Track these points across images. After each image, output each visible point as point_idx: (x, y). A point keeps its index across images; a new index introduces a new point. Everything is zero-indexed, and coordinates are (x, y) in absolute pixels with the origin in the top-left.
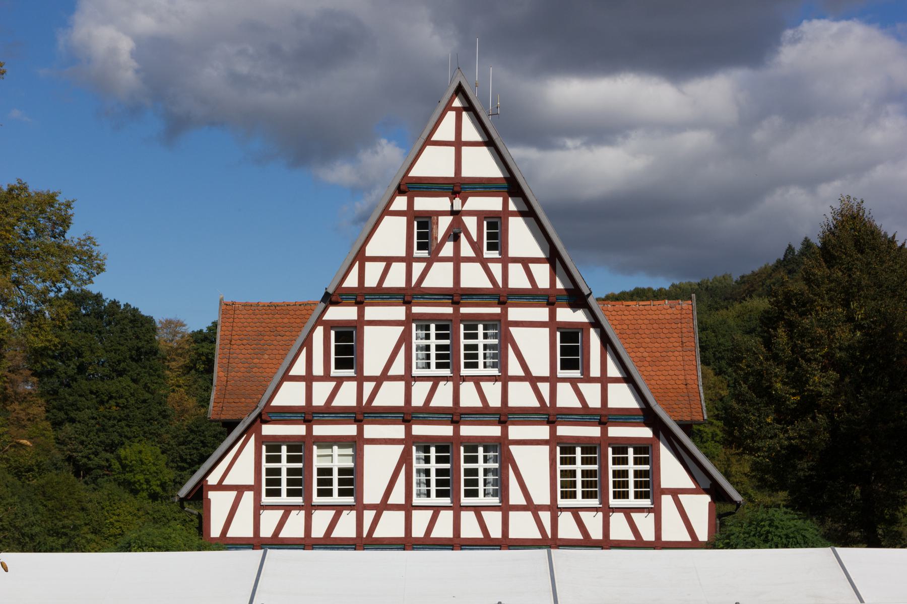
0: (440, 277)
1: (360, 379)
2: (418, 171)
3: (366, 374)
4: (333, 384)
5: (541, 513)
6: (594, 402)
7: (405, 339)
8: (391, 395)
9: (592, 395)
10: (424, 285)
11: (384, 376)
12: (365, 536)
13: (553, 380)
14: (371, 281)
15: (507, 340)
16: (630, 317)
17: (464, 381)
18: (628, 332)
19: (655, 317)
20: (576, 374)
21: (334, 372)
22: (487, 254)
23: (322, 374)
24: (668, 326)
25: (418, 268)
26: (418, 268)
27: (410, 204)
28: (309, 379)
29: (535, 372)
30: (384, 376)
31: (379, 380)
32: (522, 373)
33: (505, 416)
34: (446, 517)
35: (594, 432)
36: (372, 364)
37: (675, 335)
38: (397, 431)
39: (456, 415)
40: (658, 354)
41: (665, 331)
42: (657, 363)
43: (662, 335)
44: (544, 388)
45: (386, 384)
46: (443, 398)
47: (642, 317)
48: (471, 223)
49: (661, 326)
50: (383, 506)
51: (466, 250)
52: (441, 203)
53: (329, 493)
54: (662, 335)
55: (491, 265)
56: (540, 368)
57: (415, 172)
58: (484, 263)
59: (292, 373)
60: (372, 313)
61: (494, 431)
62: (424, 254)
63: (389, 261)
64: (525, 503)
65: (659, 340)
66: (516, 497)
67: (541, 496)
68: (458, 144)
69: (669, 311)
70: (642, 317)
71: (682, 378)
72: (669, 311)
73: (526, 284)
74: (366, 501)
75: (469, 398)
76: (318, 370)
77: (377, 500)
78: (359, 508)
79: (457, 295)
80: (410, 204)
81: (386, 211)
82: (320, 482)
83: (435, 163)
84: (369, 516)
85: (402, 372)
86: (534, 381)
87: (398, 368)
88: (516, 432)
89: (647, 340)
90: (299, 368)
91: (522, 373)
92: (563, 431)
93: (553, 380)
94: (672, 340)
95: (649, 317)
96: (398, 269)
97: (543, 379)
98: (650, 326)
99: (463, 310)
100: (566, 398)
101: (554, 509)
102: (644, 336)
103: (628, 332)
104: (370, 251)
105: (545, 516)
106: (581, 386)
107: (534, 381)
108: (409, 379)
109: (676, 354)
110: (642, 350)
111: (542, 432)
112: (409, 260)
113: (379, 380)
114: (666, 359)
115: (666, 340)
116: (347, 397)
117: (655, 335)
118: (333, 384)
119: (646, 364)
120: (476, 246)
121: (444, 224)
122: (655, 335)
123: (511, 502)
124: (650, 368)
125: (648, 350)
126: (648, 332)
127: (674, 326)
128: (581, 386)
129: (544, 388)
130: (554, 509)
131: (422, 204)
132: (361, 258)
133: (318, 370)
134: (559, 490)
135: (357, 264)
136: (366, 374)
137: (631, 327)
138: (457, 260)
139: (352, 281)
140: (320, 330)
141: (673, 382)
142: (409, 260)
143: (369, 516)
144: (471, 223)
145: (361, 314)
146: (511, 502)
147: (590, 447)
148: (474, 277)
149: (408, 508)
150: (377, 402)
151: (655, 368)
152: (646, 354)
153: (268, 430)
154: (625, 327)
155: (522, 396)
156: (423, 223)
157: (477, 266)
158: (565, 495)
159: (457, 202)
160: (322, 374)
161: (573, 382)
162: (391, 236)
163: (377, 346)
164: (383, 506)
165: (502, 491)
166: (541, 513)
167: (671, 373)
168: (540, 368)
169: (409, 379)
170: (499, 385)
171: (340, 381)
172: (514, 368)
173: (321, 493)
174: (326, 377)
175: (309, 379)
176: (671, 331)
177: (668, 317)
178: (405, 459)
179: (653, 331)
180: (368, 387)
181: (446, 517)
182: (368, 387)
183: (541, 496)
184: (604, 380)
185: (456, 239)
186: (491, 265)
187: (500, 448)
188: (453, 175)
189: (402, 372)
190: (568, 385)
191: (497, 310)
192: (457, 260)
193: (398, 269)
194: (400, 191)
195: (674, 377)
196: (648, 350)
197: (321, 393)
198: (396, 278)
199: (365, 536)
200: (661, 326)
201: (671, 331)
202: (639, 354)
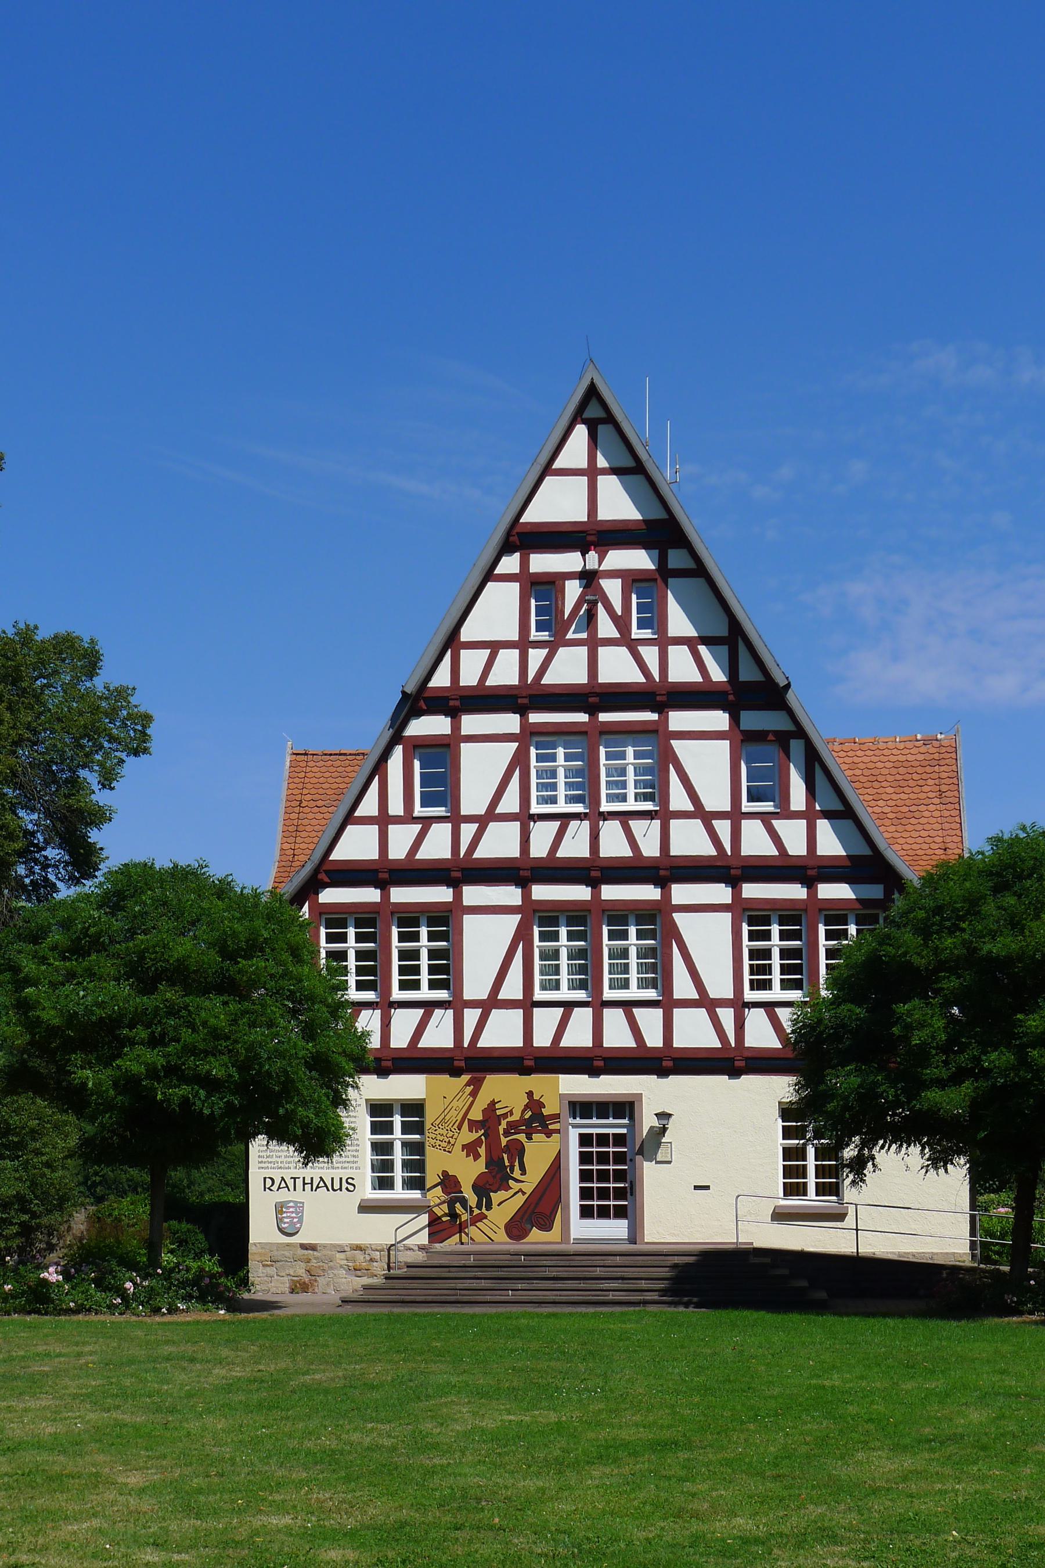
0: (568, 668)
1: (456, 819)
2: (536, 514)
3: (464, 812)
4: (418, 827)
5: (719, 1011)
6: (797, 847)
7: (520, 761)
8: (500, 843)
9: (794, 837)
10: (545, 681)
11: (490, 816)
12: (466, 1045)
13: (736, 816)
14: (469, 678)
15: (667, 758)
16: (866, 759)
17: (605, 820)
18: (863, 779)
19: (902, 758)
20: (767, 807)
21: (418, 810)
22: (636, 633)
23: (401, 812)
24: (920, 770)
25: (536, 656)
26: (536, 656)
27: (524, 563)
28: (383, 820)
29: (710, 806)
30: (490, 816)
31: (483, 821)
32: (690, 807)
33: (668, 871)
34: (583, 1017)
35: (796, 892)
36: (474, 798)
37: (930, 782)
38: (510, 895)
39: (594, 871)
40: (905, 809)
41: (916, 777)
42: (904, 821)
43: (911, 783)
44: (723, 828)
45: (495, 1013)
46: (575, 845)
47: (882, 758)
48: (613, 588)
49: (910, 770)
50: (491, 1003)
51: (606, 628)
52: (569, 561)
53: (415, 985)
54: (911, 783)
55: (642, 650)
56: (716, 799)
57: (531, 516)
58: (632, 646)
59: (358, 813)
60: (472, 723)
61: (649, 893)
62: (544, 636)
63: (494, 647)
64: (696, 996)
65: (907, 790)
66: (683, 987)
67: (720, 987)
68: (592, 473)
69: (923, 749)
70: (882, 758)
71: (939, 840)
72: (923, 749)
73: (694, 676)
74: (467, 995)
75: (614, 844)
76: (396, 807)
77: (483, 995)
78: (457, 1005)
79: (594, 697)
80: (524, 563)
81: (489, 575)
82: (402, 970)
83: (558, 503)
84: (471, 1017)
85: (519, 996)
86: (707, 818)
87: (510, 803)
88: (682, 893)
89: (890, 790)
90: (369, 806)
91: (690, 807)
92: (751, 891)
93: (736, 816)
94: (926, 789)
95: (893, 758)
96: (509, 659)
97: (721, 815)
98: (894, 771)
99: (604, 717)
100: (756, 842)
101: (740, 1006)
102: (884, 784)
103: (863, 779)
104: (467, 634)
105: (726, 1016)
106: (777, 823)
107: (707, 818)
108: (526, 818)
109: (932, 807)
110: (881, 803)
111: (720, 893)
112: (523, 645)
113: (483, 821)
114: (916, 814)
115: (917, 789)
116: (437, 846)
117: (902, 783)
118: (418, 827)
119: (887, 822)
120: (622, 623)
121: (573, 590)
122: (902, 783)
123: (676, 996)
124: (892, 828)
125: (890, 803)
126: (890, 778)
127: (929, 769)
128: (777, 823)
129: (723, 828)
130: (740, 1006)
131: (542, 563)
132: (452, 642)
133: (396, 807)
134: (747, 977)
135: (449, 652)
136: (464, 812)
137: (866, 772)
138: (593, 644)
139: (441, 679)
140: (398, 751)
141: (926, 846)
142: (523, 645)
143: (471, 1017)
144: (613, 588)
145: (456, 727)
146: (676, 996)
147: (791, 916)
148: (618, 668)
149: (528, 1005)
150: (482, 852)
151: (900, 828)
152: (887, 810)
153: (330, 896)
154: (858, 772)
155: (690, 840)
156: (542, 588)
157: (623, 651)
158: (756, 985)
159: (592, 556)
160: (401, 812)
161: (766, 818)
162: (497, 612)
163: (481, 770)
164: (491, 1003)
165: (663, 979)
166: (719, 1011)
167: (924, 834)
168: (716, 799)
169: (526, 818)
170: (657, 824)
171: (427, 822)
172: (679, 800)
173: (404, 986)
174: (408, 818)
175: (383, 820)
176: (924, 776)
177: (921, 757)
178: (522, 935)
179: (898, 777)
180: (468, 831)
181: (583, 1017)
182: (468, 831)
183: (720, 987)
184: (810, 816)
185: (592, 616)
186: (642, 650)
187: (658, 921)
188: (584, 518)
189: (519, 996)
190: (758, 823)
191: (655, 717)
192: (593, 644)
193: (509, 659)
194: (506, 548)
195: (928, 840)
196: (890, 803)
197: (400, 841)
198: (506, 672)
199: (466, 1045)
200: (910, 770)
201: (924, 776)
202: (877, 810)
